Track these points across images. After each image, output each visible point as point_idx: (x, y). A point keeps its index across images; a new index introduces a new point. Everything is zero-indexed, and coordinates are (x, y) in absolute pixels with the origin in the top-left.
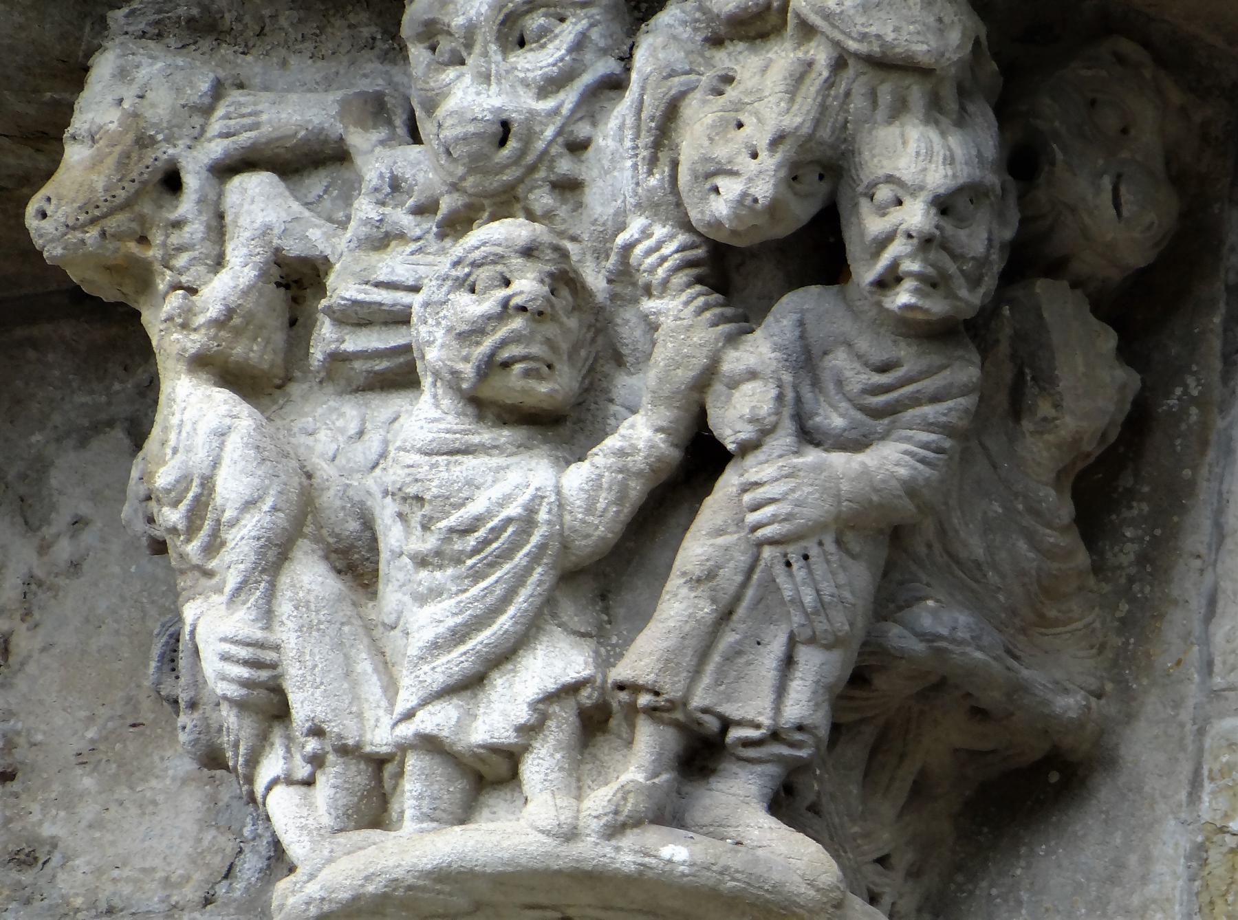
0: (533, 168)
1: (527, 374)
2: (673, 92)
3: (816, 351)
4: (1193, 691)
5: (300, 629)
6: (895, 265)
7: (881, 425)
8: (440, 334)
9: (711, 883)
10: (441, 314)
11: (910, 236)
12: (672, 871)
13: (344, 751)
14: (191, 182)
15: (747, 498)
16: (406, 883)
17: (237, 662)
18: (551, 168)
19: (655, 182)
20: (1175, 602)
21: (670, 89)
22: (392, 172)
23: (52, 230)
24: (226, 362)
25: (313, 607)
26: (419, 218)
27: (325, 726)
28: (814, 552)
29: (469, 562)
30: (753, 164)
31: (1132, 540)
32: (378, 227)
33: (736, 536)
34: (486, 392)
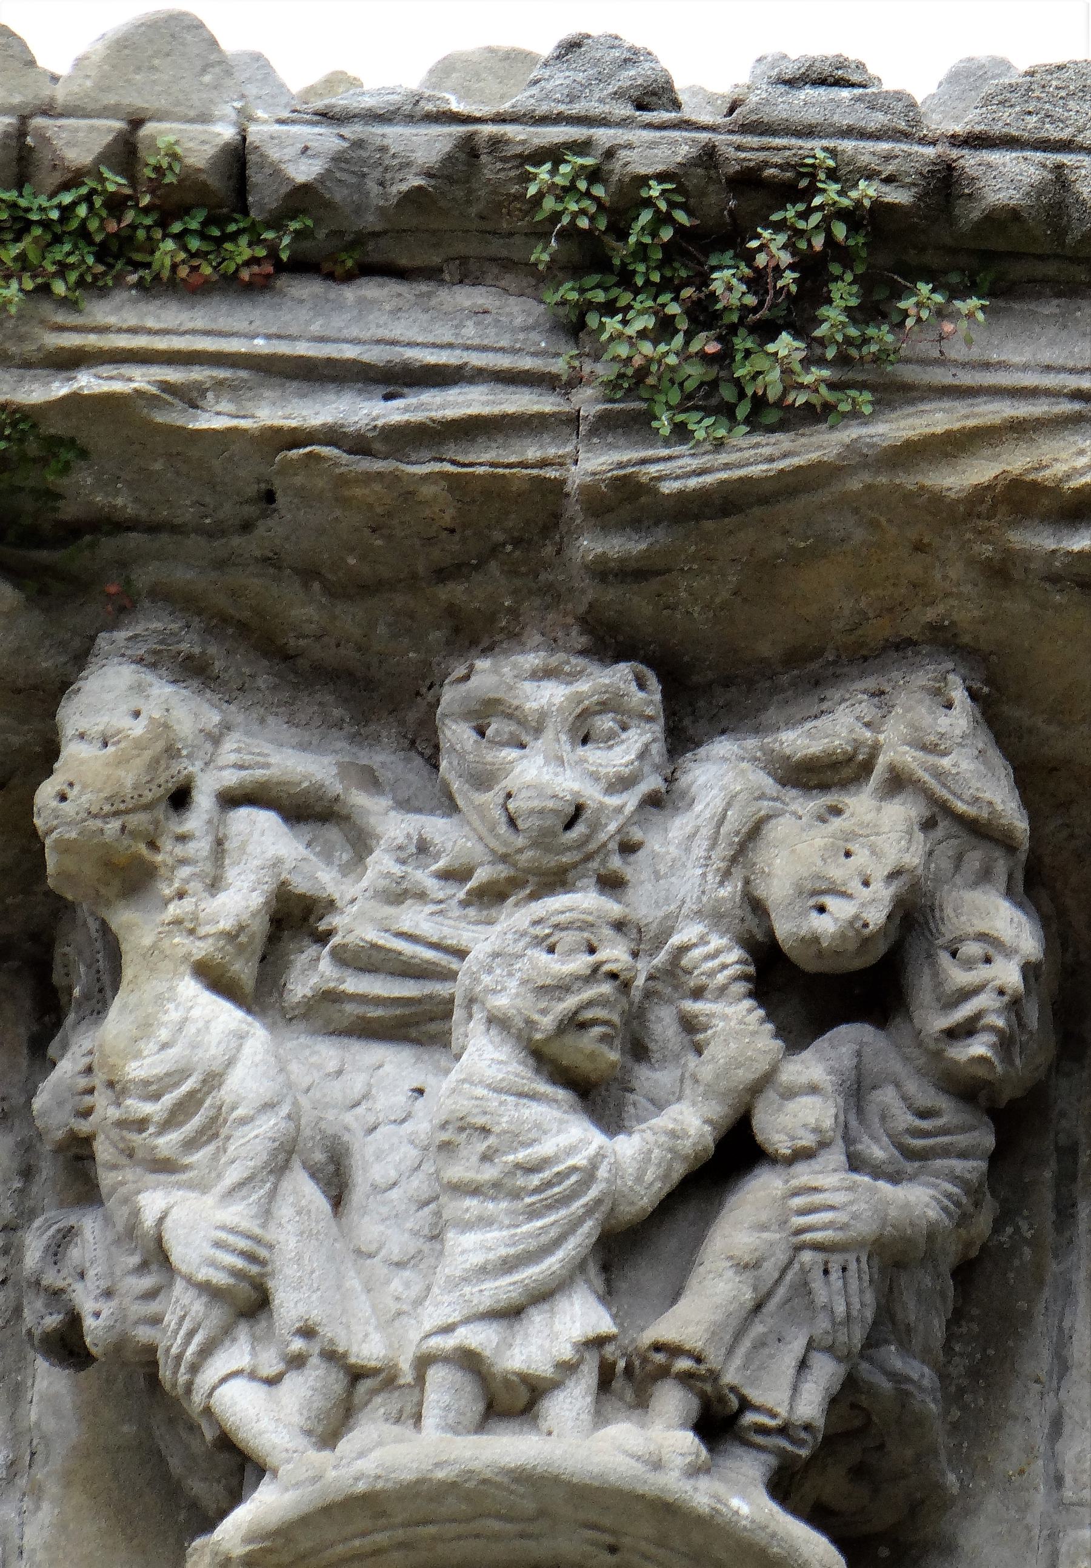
0: (589, 858)
1: (604, 1039)
2: (762, 813)
3: (867, 1082)
4: (1040, 1498)
5: (302, 1233)
6: (978, 1016)
7: (911, 1167)
8: (513, 984)
9: (763, 1543)
10: (517, 966)
11: (1001, 992)
12: (737, 1522)
13: (331, 1356)
14: (203, 801)
15: (798, 1202)
16: (482, 1476)
18: (604, 862)
20: (1015, 1418)
21: (760, 810)
22: (420, 835)
23: (72, 813)
24: (222, 975)
25: (313, 1217)
27: (319, 1329)
28: (853, 1266)
29: (528, 1200)
31: (961, 1355)
33: (778, 1236)
34: (553, 1049)
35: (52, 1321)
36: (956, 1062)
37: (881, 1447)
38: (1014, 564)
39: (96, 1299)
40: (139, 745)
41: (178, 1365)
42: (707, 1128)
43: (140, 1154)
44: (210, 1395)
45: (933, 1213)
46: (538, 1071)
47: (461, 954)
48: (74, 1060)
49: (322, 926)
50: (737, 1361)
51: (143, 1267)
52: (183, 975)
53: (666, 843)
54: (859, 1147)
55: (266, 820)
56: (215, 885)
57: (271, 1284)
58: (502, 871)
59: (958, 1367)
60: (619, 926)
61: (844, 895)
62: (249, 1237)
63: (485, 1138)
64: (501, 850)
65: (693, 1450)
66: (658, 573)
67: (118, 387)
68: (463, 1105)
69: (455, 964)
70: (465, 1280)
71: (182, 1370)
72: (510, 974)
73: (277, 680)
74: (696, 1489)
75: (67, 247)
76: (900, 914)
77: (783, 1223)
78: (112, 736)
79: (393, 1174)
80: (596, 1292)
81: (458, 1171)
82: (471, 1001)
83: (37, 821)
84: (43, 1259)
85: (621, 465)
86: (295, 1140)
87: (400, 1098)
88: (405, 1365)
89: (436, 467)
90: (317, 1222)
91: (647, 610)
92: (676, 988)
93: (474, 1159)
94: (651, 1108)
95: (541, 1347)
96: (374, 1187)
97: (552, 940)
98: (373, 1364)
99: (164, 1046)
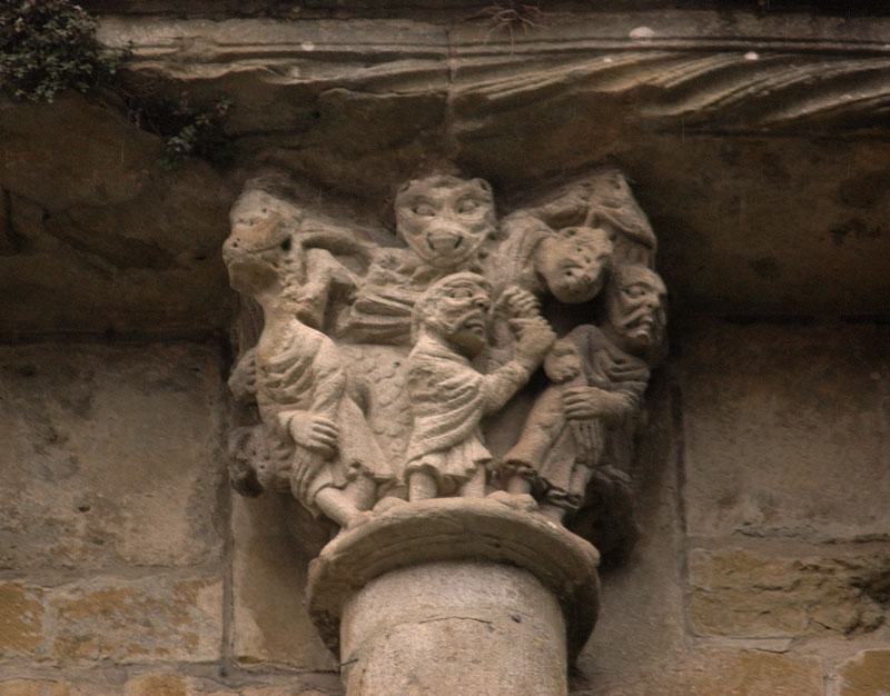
0: (466, 260)
4: (677, 536)
7: (613, 385)
8: (437, 312)
13: (369, 475)
14: (297, 246)
15: (567, 399)
35: (242, 475)
40: (267, 223)
42: (525, 371)
43: (279, 396)
45: (626, 404)
47: (411, 304)
49: (351, 297)
50: (546, 467)
51: (282, 446)
55: (324, 253)
56: (303, 281)
57: (339, 445)
61: (579, 267)
67: (249, 68)
68: (419, 362)
69: (410, 309)
70: (425, 437)
75: (166, 161)
77: (560, 410)
81: (418, 392)
87: (389, 367)
88: (400, 477)
89: (390, 95)
92: (506, 313)
99: (286, 349)
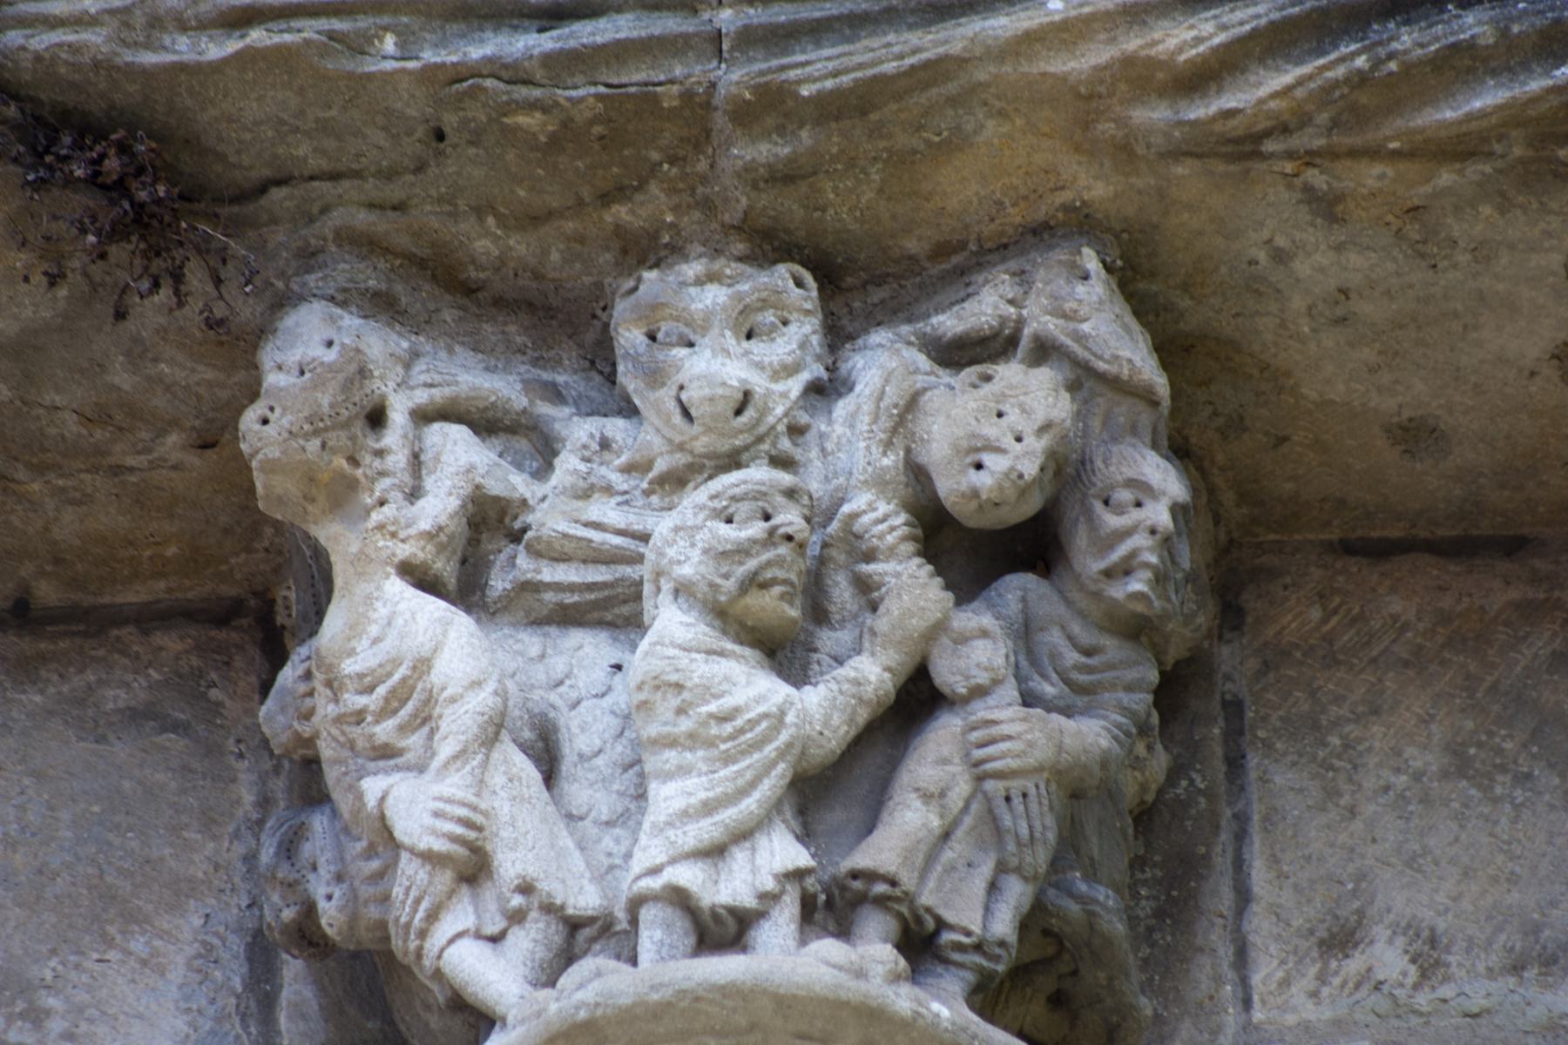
0: (760, 439)
1: (782, 597)
6: (1133, 554)
7: (1080, 701)
8: (696, 555)
11: (1153, 532)
13: (549, 909)
14: (398, 416)
15: (975, 736)
17: (451, 819)
18: (774, 444)
19: (890, 463)
20: (1201, 950)
22: (602, 433)
24: (426, 574)
25: (525, 783)
26: (626, 476)
27: (539, 885)
29: (723, 747)
30: (1018, 446)
31: (1147, 898)
32: (585, 479)
36: (1115, 600)
37: (1075, 973)
38: (1136, 140)
39: (328, 884)
41: (407, 933)
42: (887, 675)
44: (439, 957)
45: (1105, 742)
46: (724, 632)
47: (644, 538)
48: (294, 668)
49: (517, 525)
50: (931, 884)
52: (388, 576)
53: (830, 422)
54: (1031, 684)
55: (459, 432)
56: (414, 494)
58: (681, 459)
59: (1145, 908)
60: (791, 494)
61: (999, 450)
62: (464, 804)
63: (680, 693)
64: (678, 439)
65: (892, 958)
66: (804, 177)
68: (656, 665)
70: (670, 824)
71: (412, 937)
72: (693, 545)
73: (461, 313)
74: (897, 995)
76: (1052, 466)
78: (308, 364)
79: (598, 743)
80: (794, 832)
82: (659, 574)
83: (243, 446)
84: (277, 854)
85: (762, 73)
86: (503, 714)
88: (621, 914)
90: (528, 787)
91: (799, 213)
93: (670, 715)
94: (835, 664)
95: (744, 881)
96: (581, 756)
97: (731, 510)
98: (590, 913)
